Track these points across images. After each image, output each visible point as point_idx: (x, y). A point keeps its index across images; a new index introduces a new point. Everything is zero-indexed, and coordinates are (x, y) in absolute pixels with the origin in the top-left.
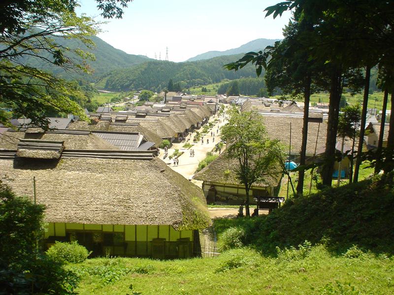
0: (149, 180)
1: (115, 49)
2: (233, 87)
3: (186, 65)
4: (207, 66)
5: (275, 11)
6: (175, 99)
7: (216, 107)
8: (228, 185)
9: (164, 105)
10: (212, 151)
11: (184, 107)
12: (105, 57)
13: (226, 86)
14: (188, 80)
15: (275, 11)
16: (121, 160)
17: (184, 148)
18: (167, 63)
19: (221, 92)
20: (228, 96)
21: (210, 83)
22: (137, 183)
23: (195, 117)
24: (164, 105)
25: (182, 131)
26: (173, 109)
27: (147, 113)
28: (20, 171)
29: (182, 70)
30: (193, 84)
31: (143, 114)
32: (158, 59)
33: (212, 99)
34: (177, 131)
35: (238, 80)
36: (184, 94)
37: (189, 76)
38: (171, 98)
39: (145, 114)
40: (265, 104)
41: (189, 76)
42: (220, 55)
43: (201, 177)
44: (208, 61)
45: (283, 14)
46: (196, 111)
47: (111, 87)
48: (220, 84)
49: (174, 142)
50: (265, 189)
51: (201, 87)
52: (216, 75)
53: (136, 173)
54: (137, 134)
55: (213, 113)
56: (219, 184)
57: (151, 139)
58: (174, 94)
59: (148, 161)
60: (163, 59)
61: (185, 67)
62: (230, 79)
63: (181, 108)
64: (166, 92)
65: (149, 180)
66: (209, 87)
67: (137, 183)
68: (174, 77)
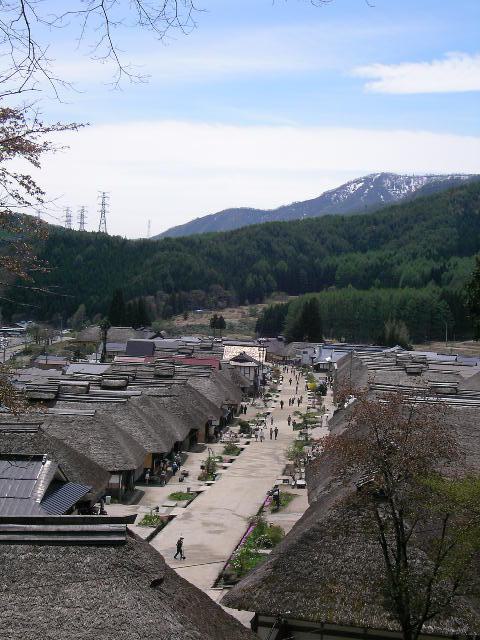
0: (113, 611)
3: (163, 249)
4: (224, 252)
6: (133, 349)
7: (256, 376)
8: (334, 628)
9: (104, 368)
10: (261, 511)
11: (165, 373)
13: (282, 311)
16: (26, 547)
17: (173, 503)
18: (102, 241)
20: (288, 341)
22: (77, 624)
23: (199, 404)
24: (104, 368)
25: (165, 449)
26: (132, 379)
27: (58, 395)
29: (148, 262)
30: (179, 308)
31: (46, 396)
32: (76, 227)
33: (246, 349)
34: (151, 448)
36: (158, 335)
37: (170, 281)
38: (123, 347)
39: (52, 396)
40: (405, 369)
41: (170, 281)
42: (262, 220)
43: (250, 599)
46: (204, 385)
48: (260, 308)
49: (142, 481)
53: (74, 592)
54: (39, 458)
55: (254, 392)
56: (306, 624)
57: (75, 474)
58: (130, 335)
59: (112, 550)
60: (92, 226)
61: (159, 255)
63: (158, 376)
64: (105, 328)
65: (113, 611)
67: (77, 624)
68: (125, 285)
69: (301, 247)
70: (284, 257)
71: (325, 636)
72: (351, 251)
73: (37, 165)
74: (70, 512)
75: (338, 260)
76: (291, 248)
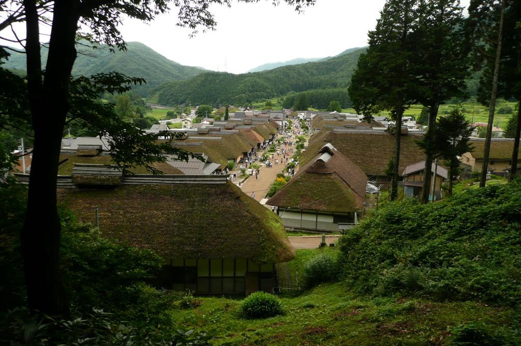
1: (168, 60)
2: (301, 100)
5: (43, 67)
12: (157, 69)
14: (251, 93)
15: (43, 67)
18: (226, 75)
19: (288, 105)
21: (273, 96)
28: (213, 302)
35: (305, 92)
36: (246, 109)
37: (251, 89)
41: (251, 89)
42: (207, 72)
44: (271, 71)
45: (380, 14)
47: (163, 102)
50: (347, 214)
51: (265, 101)
52: (281, 86)
62: (296, 92)
66: (274, 101)
69: (300, 74)
70: (294, 78)
71: (303, 214)
72: (319, 75)
73: (7, 60)
74: (213, 173)
75: (322, 77)
76: (296, 74)
